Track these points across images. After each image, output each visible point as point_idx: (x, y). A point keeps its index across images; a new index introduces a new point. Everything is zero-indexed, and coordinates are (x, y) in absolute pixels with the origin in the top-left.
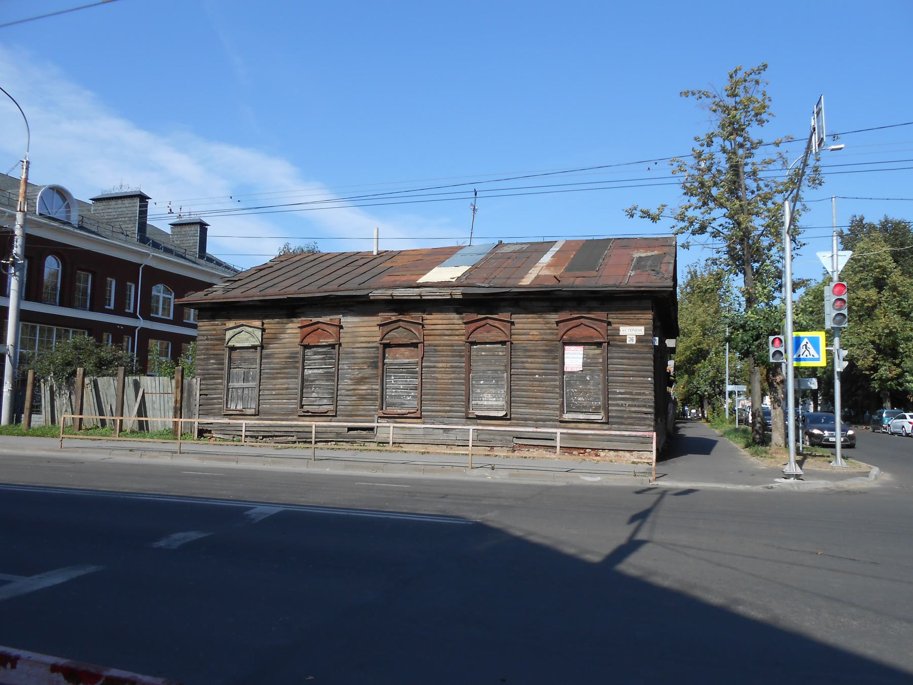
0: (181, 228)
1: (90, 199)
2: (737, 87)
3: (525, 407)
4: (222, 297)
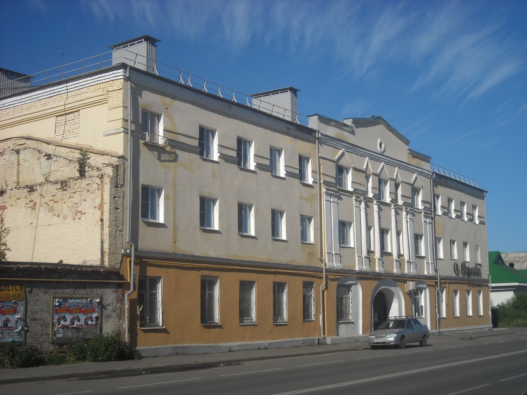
0: (61, 179)
1: (161, 41)
2: (75, 330)
3: (351, 148)
4: (52, 226)
